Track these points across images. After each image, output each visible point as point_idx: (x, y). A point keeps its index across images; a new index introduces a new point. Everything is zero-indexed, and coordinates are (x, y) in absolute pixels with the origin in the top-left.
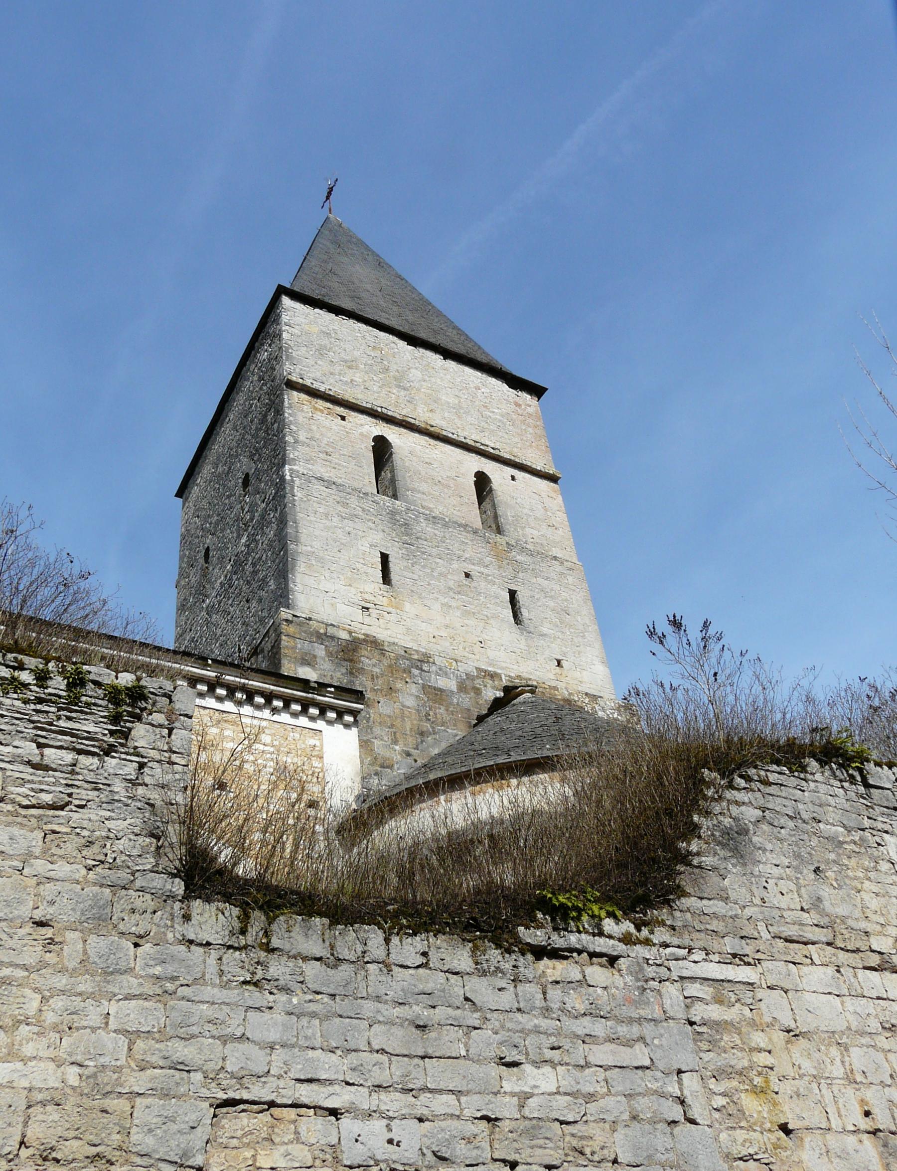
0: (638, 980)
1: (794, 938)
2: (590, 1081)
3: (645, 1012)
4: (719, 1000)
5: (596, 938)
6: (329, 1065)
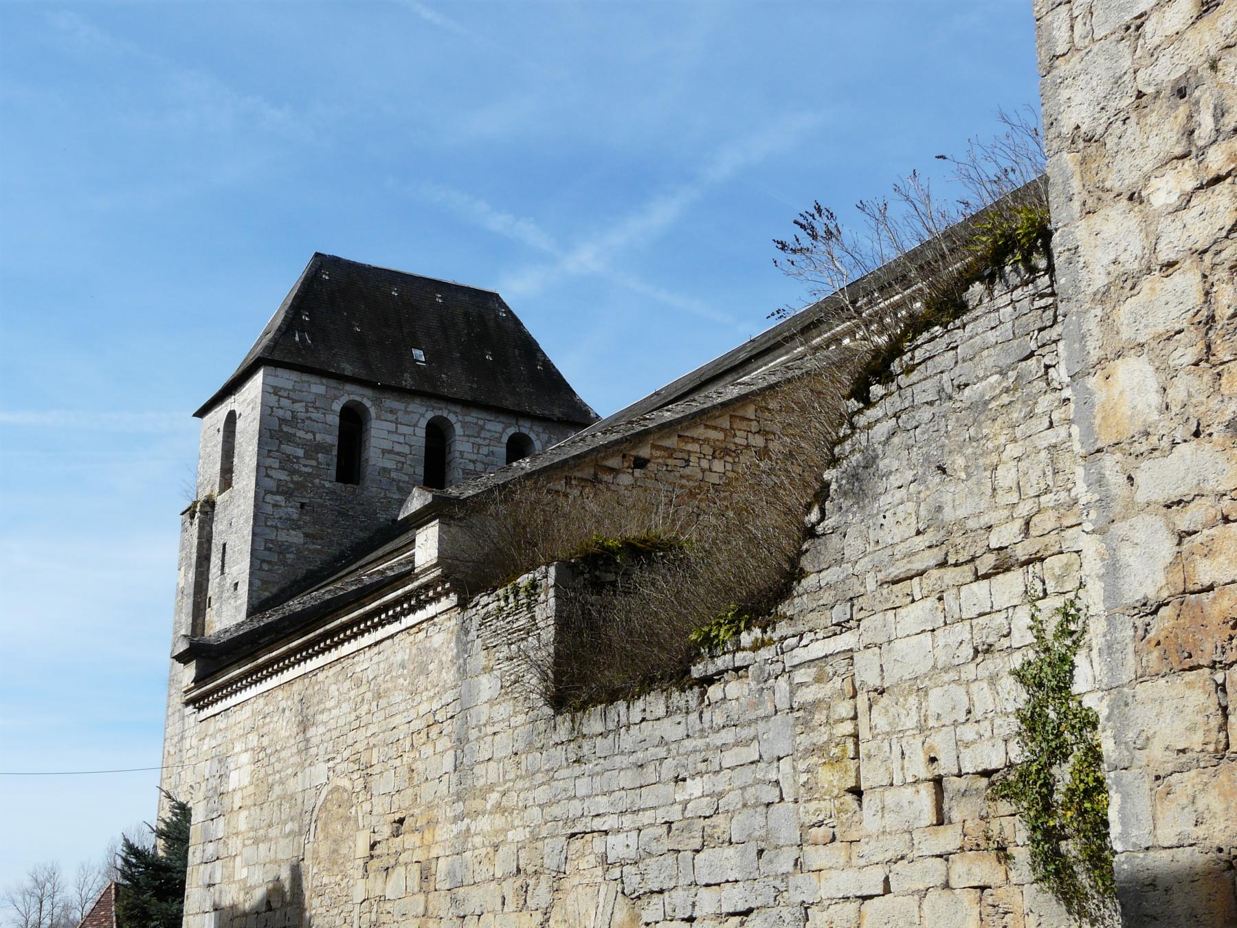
0: (759, 683)
1: (902, 576)
2: (721, 782)
3: (761, 712)
4: (818, 680)
5: (1016, 696)
6: (602, 803)
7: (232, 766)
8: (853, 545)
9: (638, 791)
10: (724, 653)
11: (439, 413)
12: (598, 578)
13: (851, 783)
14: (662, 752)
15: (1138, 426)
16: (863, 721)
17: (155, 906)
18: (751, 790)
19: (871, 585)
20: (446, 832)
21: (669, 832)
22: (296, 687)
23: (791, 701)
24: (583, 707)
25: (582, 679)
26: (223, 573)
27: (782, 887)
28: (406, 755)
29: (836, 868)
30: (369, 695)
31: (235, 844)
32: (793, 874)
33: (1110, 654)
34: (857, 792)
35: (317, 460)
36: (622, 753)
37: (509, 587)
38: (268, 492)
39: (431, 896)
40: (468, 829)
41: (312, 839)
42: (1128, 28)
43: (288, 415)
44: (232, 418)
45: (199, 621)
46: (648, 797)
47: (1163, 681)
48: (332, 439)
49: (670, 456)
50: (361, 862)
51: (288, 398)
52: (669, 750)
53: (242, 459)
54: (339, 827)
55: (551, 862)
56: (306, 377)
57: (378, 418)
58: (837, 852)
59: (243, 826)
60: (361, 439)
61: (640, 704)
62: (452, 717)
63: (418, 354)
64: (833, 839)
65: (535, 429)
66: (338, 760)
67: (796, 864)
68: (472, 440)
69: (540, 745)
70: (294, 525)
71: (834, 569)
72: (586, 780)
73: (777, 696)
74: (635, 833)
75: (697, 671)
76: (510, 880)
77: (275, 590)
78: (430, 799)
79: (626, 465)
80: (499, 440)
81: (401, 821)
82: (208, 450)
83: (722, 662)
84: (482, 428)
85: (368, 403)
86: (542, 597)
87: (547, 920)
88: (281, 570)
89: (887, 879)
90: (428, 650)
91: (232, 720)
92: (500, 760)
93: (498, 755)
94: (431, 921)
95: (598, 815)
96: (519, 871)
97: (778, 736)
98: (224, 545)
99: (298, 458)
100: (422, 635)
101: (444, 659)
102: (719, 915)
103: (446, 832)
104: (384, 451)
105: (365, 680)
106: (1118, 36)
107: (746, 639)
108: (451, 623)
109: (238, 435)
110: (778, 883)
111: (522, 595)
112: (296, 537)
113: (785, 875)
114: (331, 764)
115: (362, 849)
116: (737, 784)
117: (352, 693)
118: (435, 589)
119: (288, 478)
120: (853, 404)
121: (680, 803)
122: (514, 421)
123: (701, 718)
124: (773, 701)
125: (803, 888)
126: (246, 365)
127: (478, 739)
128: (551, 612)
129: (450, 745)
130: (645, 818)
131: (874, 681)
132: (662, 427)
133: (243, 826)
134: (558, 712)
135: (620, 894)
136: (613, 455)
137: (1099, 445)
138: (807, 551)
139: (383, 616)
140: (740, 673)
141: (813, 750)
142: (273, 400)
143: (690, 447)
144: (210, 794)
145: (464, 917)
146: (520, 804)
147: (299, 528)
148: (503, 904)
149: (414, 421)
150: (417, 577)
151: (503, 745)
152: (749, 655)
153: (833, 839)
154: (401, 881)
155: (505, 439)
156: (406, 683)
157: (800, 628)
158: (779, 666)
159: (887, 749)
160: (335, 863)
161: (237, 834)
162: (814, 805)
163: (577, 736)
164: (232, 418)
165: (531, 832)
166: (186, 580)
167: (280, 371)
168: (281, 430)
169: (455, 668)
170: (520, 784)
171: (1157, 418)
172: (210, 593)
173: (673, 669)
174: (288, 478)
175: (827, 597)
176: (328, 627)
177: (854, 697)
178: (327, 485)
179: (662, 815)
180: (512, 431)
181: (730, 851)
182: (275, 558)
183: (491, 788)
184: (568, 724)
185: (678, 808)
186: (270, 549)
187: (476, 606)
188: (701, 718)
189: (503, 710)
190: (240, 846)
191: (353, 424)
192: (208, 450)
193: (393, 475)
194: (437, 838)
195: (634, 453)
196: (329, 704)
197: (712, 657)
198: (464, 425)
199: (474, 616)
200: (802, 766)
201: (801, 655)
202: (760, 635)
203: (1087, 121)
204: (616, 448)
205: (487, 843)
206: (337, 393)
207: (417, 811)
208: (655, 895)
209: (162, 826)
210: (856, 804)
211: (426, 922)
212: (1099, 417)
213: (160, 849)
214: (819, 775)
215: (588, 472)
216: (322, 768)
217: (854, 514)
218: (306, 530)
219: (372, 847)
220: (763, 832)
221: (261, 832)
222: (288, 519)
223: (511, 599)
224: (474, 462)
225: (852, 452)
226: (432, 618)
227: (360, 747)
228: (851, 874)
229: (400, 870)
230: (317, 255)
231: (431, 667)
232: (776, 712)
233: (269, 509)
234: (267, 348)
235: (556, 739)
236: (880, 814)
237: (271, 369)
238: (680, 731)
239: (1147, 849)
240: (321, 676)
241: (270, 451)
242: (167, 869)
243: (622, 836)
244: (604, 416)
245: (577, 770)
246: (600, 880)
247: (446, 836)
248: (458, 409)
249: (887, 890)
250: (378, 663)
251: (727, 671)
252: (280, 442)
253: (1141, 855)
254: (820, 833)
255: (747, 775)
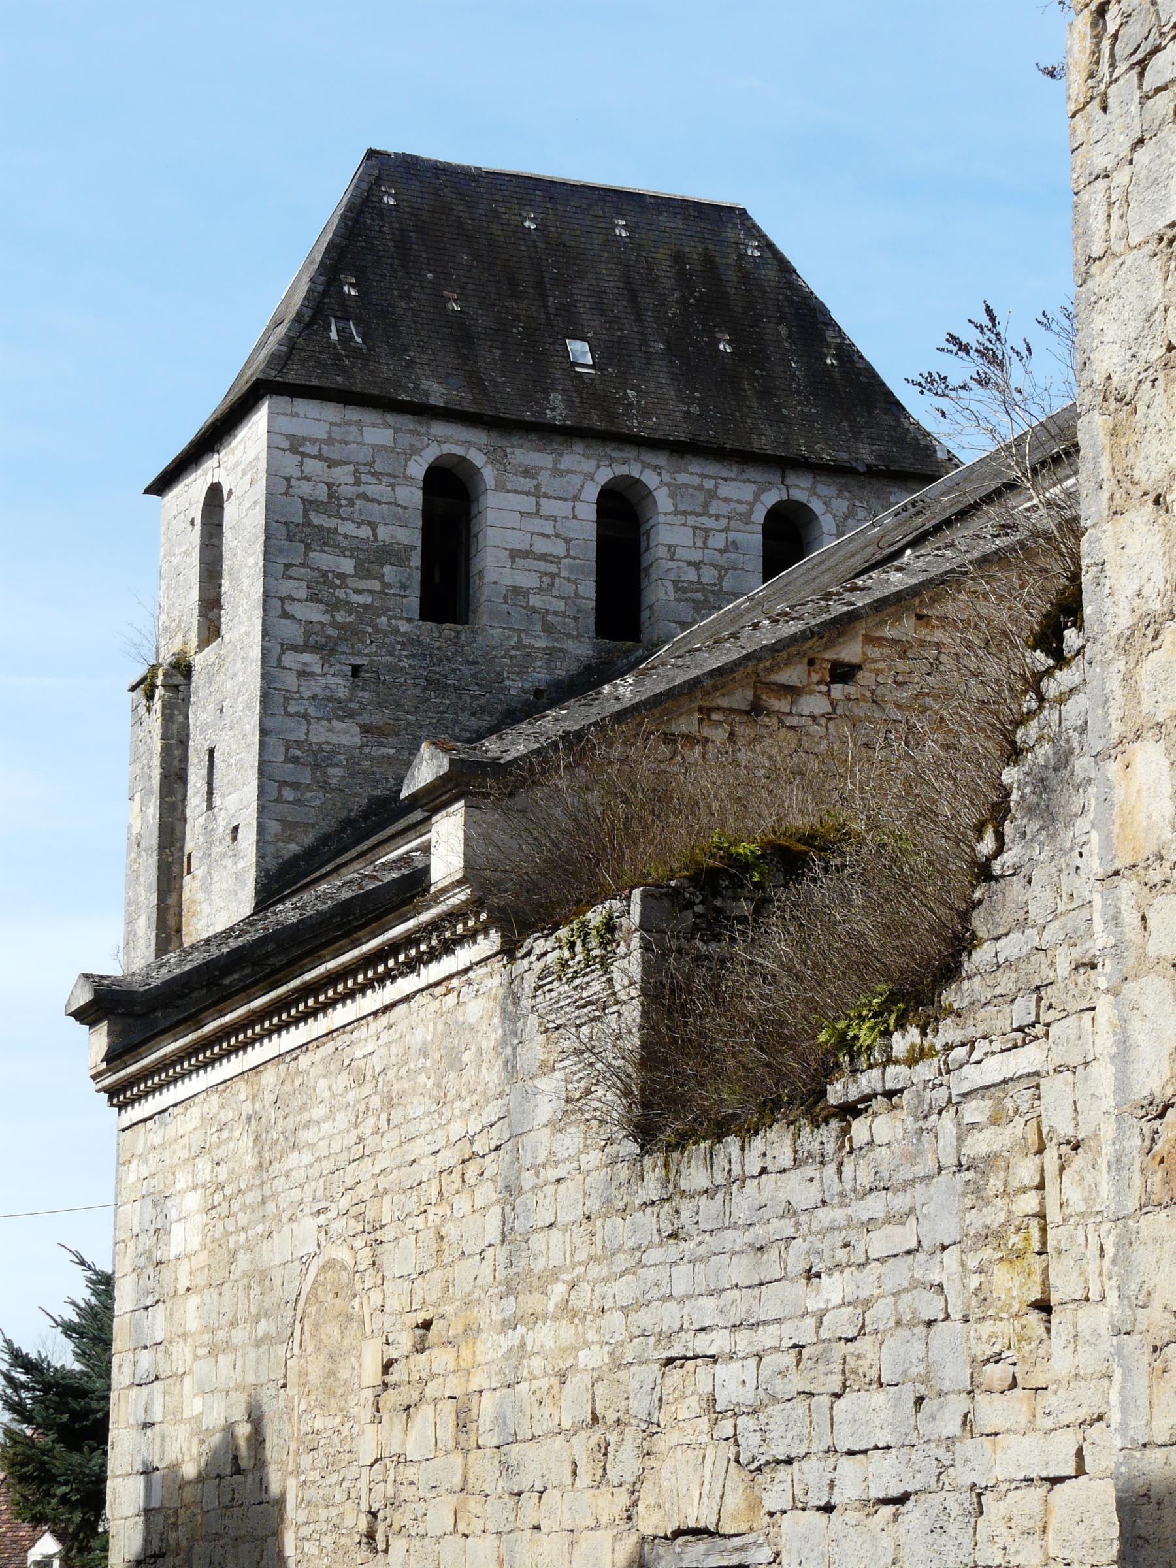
3: (919, 1170)
6: (707, 1310)
7: (173, 1215)
8: (1040, 900)
9: (756, 1291)
10: (871, 1066)
11: (622, 470)
12: (719, 911)
13: (1035, 1294)
14: (787, 1228)
15: (1150, 849)
16: (1051, 1188)
17: (64, 1459)
18: (906, 1298)
19: (1063, 969)
20: (491, 1347)
21: (799, 1362)
22: (269, 1077)
23: (959, 1152)
24: (680, 1143)
25: (701, 1082)
26: (210, 807)
27: (946, 1459)
28: (432, 1210)
29: (1016, 1432)
30: (375, 1101)
31: (182, 1353)
32: (961, 1439)
33: (1118, 1170)
34: (1043, 1306)
35: (381, 578)
36: (735, 1226)
37: (575, 926)
38: (287, 647)
39: (471, 1457)
40: (523, 1345)
41: (296, 1351)
42: (1161, 239)
43: (321, 493)
44: (215, 497)
45: (172, 901)
46: (771, 1303)
47: (1163, 1214)
48: (410, 535)
49: (903, 655)
50: (369, 1395)
51: (319, 457)
52: (798, 1225)
53: (236, 581)
54: (337, 1331)
55: (640, 1406)
56: (353, 414)
57: (501, 487)
58: (1017, 1406)
59: (193, 1324)
60: (469, 529)
61: (757, 1144)
62: (498, 1148)
63: (579, 350)
64: (1014, 1385)
65: (822, 490)
66: (332, 1214)
67: (964, 1423)
68: (691, 520)
69: (621, 1205)
70: (342, 710)
71: (1015, 936)
72: (684, 1269)
73: (941, 1143)
74: (753, 1362)
75: (836, 1093)
76: (583, 1434)
77: (308, 839)
78: (468, 1289)
79: (815, 677)
80: (747, 518)
81: (427, 1325)
82: (176, 560)
83: (869, 1081)
84: (712, 495)
85: (477, 458)
86: (622, 950)
87: (635, 1504)
88: (316, 799)
89: (1079, 1453)
90: (461, 1027)
91: (171, 1131)
92: (566, 1228)
93: (563, 1219)
94: (472, 1499)
95: (703, 1329)
96: (595, 1419)
97: (942, 1211)
98: (211, 751)
99: (342, 576)
100: (451, 999)
101: (484, 1044)
102: (865, 1503)
103: (491, 1347)
104: (514, 554)
105: (369, 1074)
106: (1147, 249)
107: (900, 1044)
108: (492, 980)
109: (228, 534)
110: (940, 1452)
111: (594, 942)
112: (346, 735)
113: (951, 1439)
114: (322, 1219)
115: (371, 1373)
116: (889, 1286)
117: (351, 1096)
118: (418, 947)
119: (326, 619)
120: (1041, 660)
121: (814, 1314)
122: (777, 478)
123: (840, 1172)
124: (935, 1152)
125: (980, 1463)
126: (234, 397)
127: (534, 1189)
128: (636, 971)
129: (494, 1196)
130: (767, 1337)
131: (1065, 1129)
132: (881, 605)
133: (193, 1324)
134: (645, 1151)
135: (733, 1463)
136: (788, 662)
137: (1117, 865)
138: (980, 902)
139: (391, 963)
140: (895, 1099)
141: (987, 1237)
142: (290, 463)
143: (939, 635)
144: (142, 1261)
145: (519, 1494)
146: (596, 1305)
147: (351, 715)
148: (574, 1473)
149: (572, 491)
150: (436, 900)
151: (568, 1202)
152: (901, 1069)
153: (1014, 1385)
154: (427, 1430)
155: (759, 515)
156: (430, 1083)
157: (972, 1032)
158: (941, 1095)
159: (1082, 1240)
160: (331, 1394)
161: (184, 1336)
162: (987, 1328)
163: (671, 1194)
164: (215, 497)
165: (611, 1354)
166: (144, 820)
167: (303, 406)
168: (308, 523)
169: (500, 1062)
170: (595, 1271)
171: (1170, 836)
172: (189, 846)
173: (801, 1089)
174: (326, 619)
175: (1006, 983)
176: (308, 977)
177: (1040, 1152)
178: (404, 627)
179: (790, 1333)
180: (772, 497)
181: (878, 1398)
182: (306, 777)
183: (554, 1274)
184: (660, 1172)
185: (811, 1321)
186: (295, 760)
187: (528, 954)
188: (840, 1172)
189: (572, 1139)
190: (189, 1357)
191: (450, 498)
192: (176, 560)
193: (535, 600)
194: (480, 1358)
195: (830, 655)
196: (318, 1112)
197: (854, 1071)
198: (675, 491)
199: (528, 969)
200: (972, 1262)
201: (973, 1077)
202: (917, 1040)
203: (1119, 370)
204: (793, 650)
205: (549, 1369)
206: (414, 440)
207: (449, 1309)
208: (782, 1467)
209: (72, 1316)
210: (1042, 1326)
211: (466, 1501)
212: (1118, 822)
213: (63, 1355)
214: (995, 1279)
215: (741, 698)
216: (308, 1225)
217: (1042, 845)
218: (365, 718)
219: (387, 1367)
220: (921, 1369)
221: (221, 1335)
222: (329, 699)
223: (579, 948)
224: (697, 565)
225: (1040, 739)
226: (466, 971)
227: (364, 1191)
228: (1032, 1441)
229: (427, 1410)
230: (371, 154)
231: (467, 1057)
232: (940, 1169)
233: (290, 681)
234: (273, 359)
235: (644, 1195)
236: (1072, 1346)
237: (282, 402)
238: (812, 1195)
239: (1144, 1445)
240: (304, 1061)
241: (287, 566)
242: (81, 1393)
243: (736, 1365)
244: (968, 458)
245: (673, 1250)
246: (705, 1438)
247: (491, 1355)
248: (661, 459)
249: (1081, 1471)
250: (388, 1044)
251: (874, 1095)
252: (308, 547)
253: (1138, 1454)
254: (996, 1373)
255: (898, 1273)
